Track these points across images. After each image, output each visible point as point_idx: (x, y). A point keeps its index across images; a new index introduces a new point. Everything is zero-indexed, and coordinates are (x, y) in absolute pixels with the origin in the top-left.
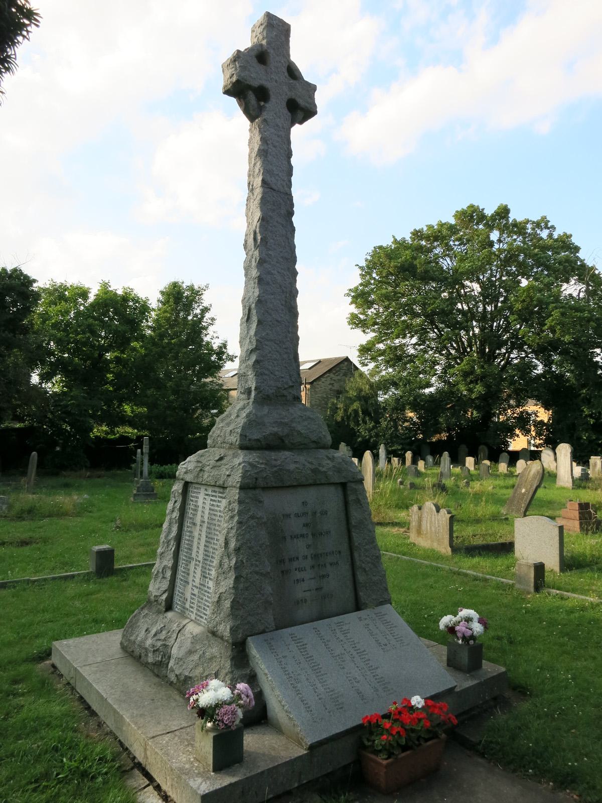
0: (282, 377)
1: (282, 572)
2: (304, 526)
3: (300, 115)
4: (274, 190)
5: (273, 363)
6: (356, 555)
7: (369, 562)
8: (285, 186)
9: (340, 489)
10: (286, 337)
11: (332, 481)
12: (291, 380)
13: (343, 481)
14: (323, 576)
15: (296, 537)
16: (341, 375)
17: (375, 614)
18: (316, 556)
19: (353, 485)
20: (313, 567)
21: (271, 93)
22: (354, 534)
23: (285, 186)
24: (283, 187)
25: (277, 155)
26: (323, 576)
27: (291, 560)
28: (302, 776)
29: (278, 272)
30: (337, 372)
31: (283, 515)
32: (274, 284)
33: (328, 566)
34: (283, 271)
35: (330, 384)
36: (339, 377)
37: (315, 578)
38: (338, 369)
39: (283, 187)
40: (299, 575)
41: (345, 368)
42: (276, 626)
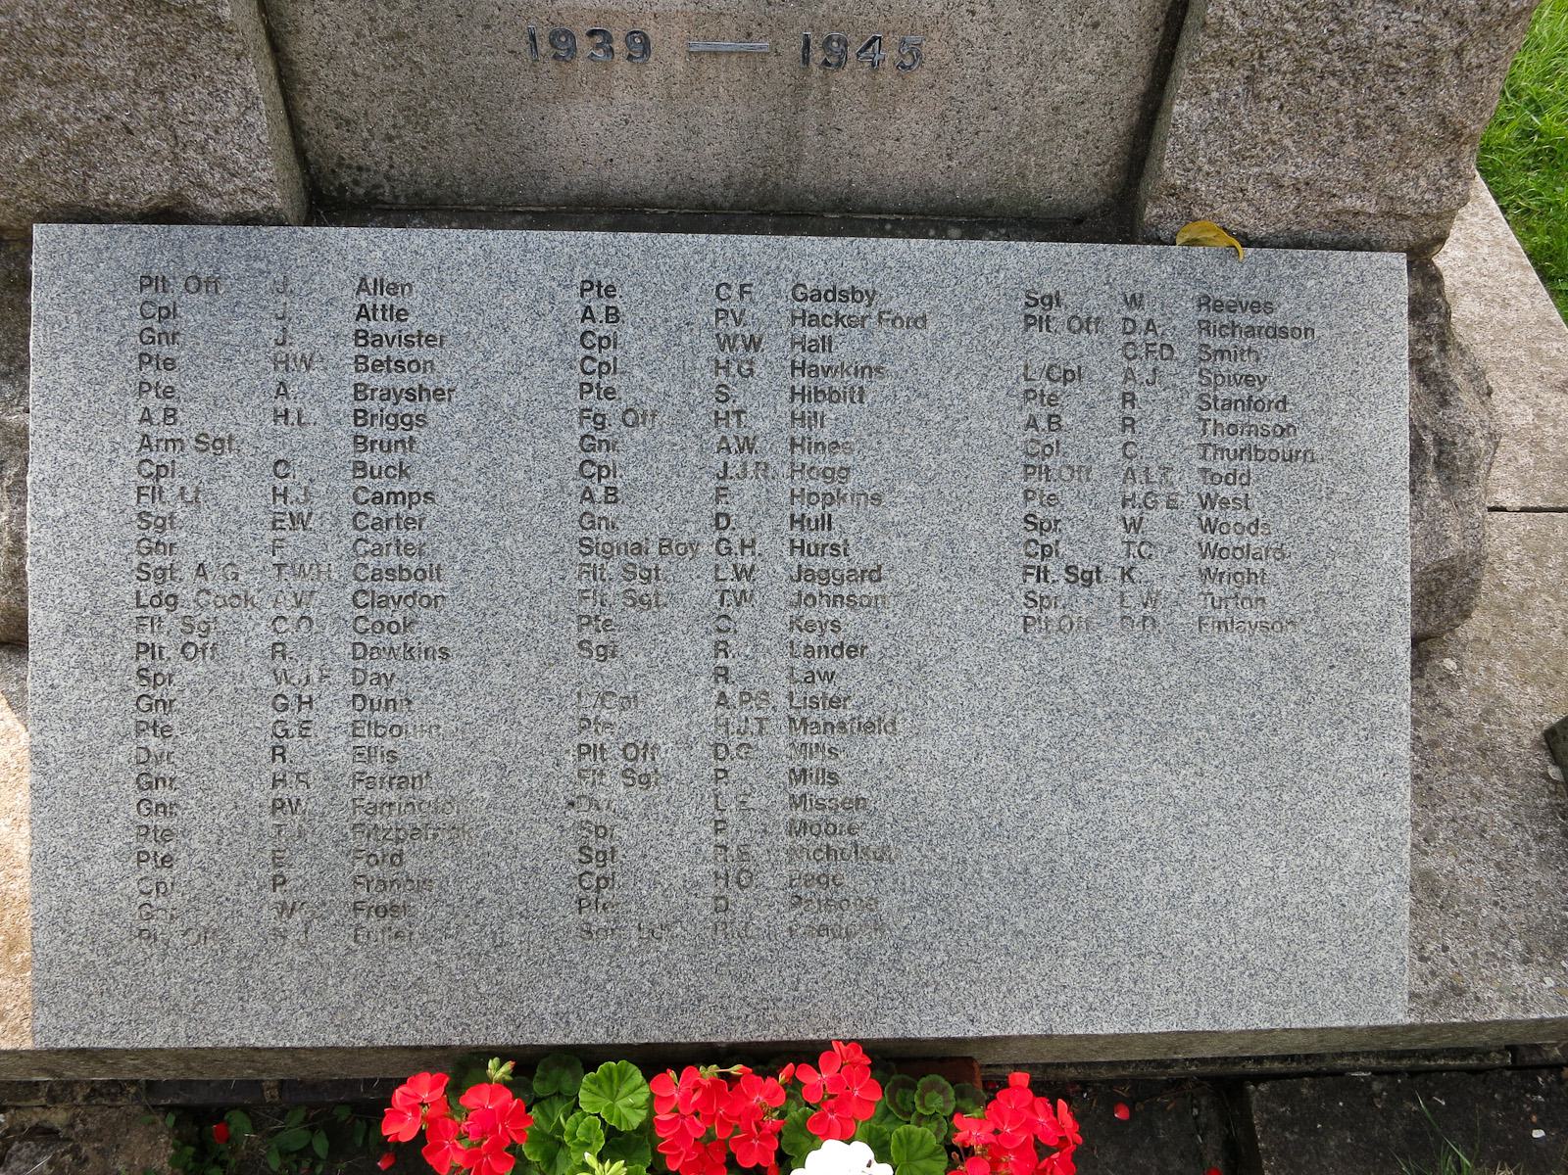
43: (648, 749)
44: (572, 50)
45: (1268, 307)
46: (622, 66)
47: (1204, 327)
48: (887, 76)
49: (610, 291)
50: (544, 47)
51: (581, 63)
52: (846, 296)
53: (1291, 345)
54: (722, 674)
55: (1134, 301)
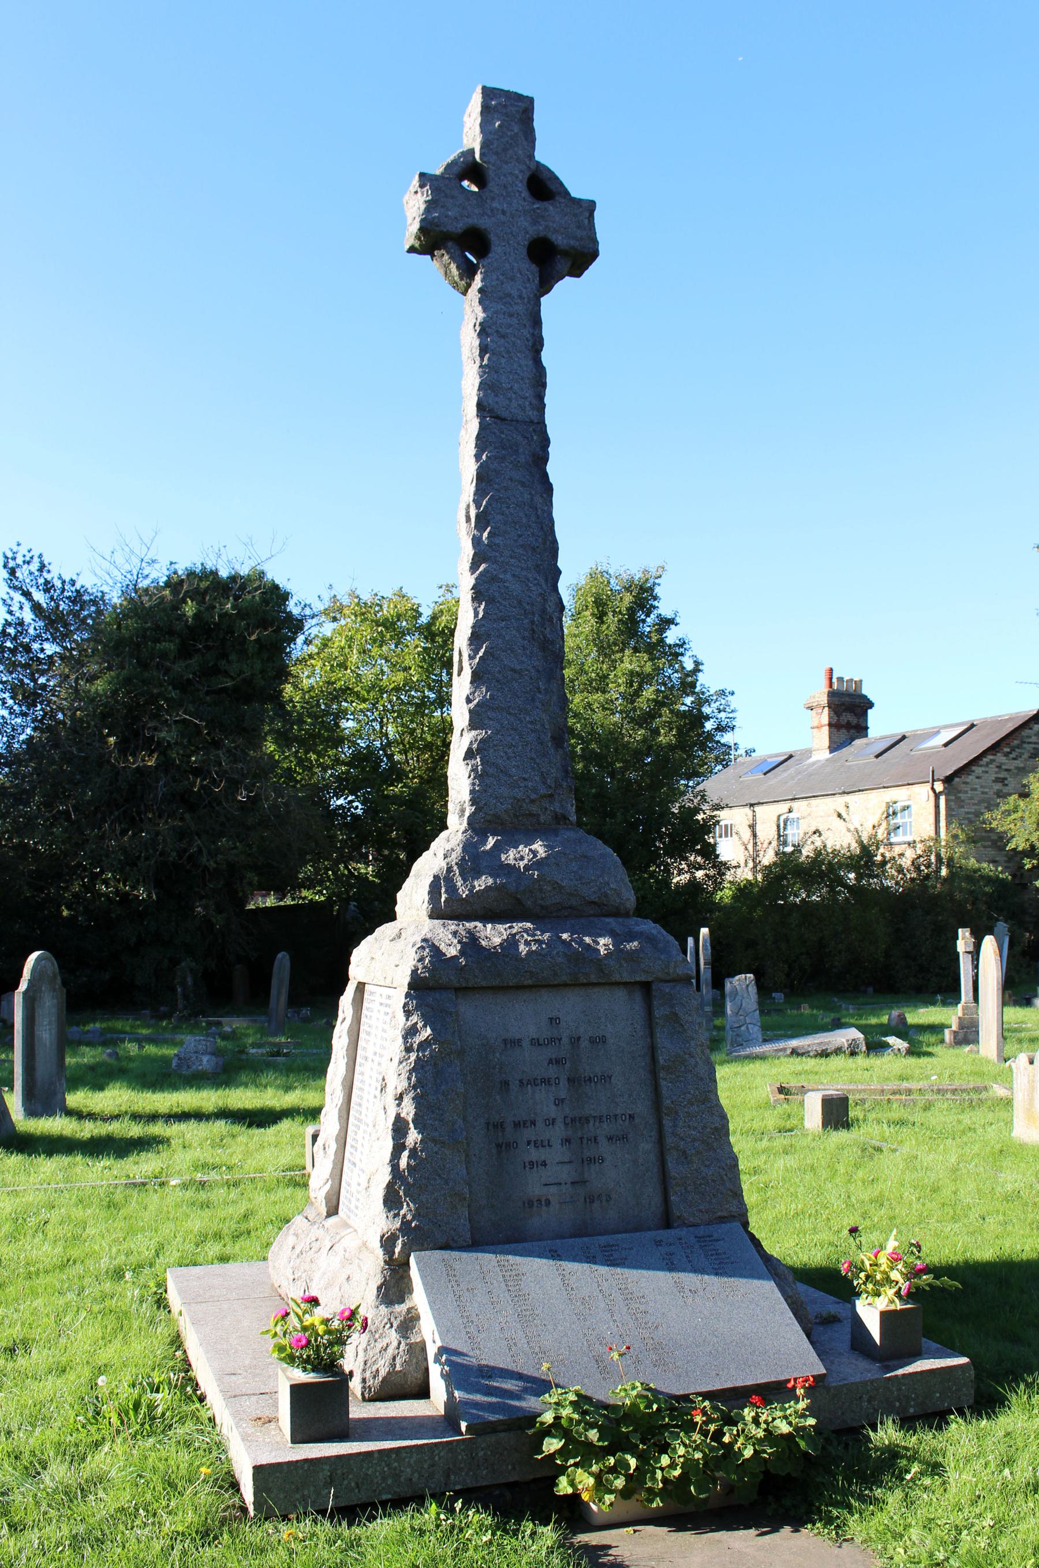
0: (525, 779)
1: (499, 1146)
2: (550, 1061)
3: (562, 264)
4: (503, 420)
5: (506, 752)
6: (667, 1122)
7: (694, 1140)
8: (528, 408)
9: (638, 996)
10: (533, 700)
11: (616, 978)
12: (544, 783)
13: (641, 977)
14: (591, 1160)
15: (534, 1082)
16: (1026, 756)
17: (696, 1237)
18: (577, 1121)
19: (667, 988)
20: (567, 1141)
21: (492, 237)
22: (663, 1083)
23: (528, 408)
24: (524, 410)
25: (508, 352)
26: (591, 1160)
27: (517, 1125)
28: (452, 1477)
29: (514, 575)
30: (1013, 750)
31: (505, 1041)
32: (505, 599)
33: (603, 1141)
34: (524, 573)
35: (998, 780)
36: (1019, 763)
37: (570, 1162)
38: (1016, 742)
39: (524, 410)
40: (534, 1154)
41: (1034, 739)
42: (473, 1238)
43: (27, 1350)
44: (533, 1205)
45: (712, 1236)
46: (544, 1208)
47: (698, 1242)
48: (604, 1203)
49: (556, 1251)
50: (526, 1205)
51: (535, 1208)
52: (612, 1246)
53: (721, 1242)
54: (615, 1321)
55: (680, 1239)
